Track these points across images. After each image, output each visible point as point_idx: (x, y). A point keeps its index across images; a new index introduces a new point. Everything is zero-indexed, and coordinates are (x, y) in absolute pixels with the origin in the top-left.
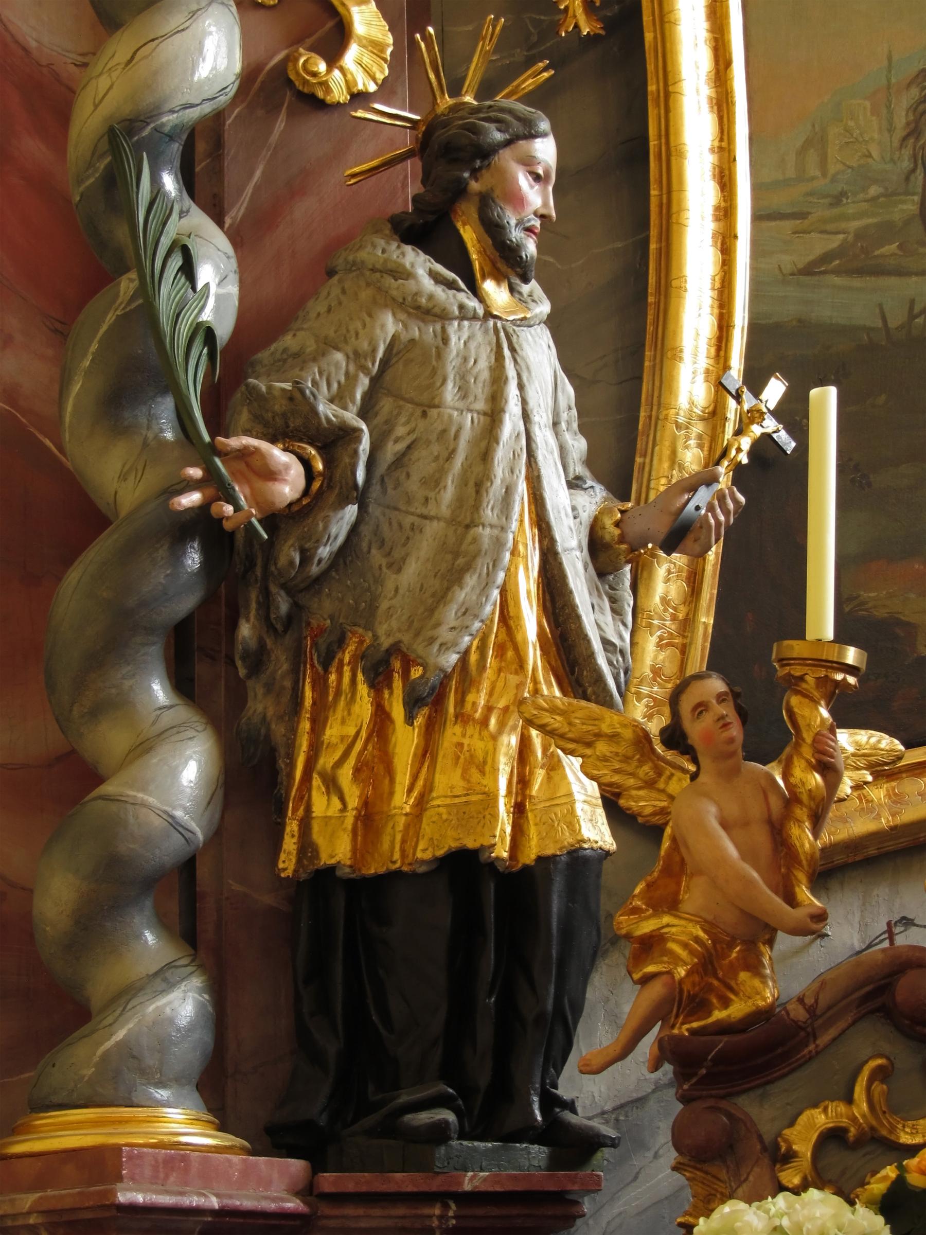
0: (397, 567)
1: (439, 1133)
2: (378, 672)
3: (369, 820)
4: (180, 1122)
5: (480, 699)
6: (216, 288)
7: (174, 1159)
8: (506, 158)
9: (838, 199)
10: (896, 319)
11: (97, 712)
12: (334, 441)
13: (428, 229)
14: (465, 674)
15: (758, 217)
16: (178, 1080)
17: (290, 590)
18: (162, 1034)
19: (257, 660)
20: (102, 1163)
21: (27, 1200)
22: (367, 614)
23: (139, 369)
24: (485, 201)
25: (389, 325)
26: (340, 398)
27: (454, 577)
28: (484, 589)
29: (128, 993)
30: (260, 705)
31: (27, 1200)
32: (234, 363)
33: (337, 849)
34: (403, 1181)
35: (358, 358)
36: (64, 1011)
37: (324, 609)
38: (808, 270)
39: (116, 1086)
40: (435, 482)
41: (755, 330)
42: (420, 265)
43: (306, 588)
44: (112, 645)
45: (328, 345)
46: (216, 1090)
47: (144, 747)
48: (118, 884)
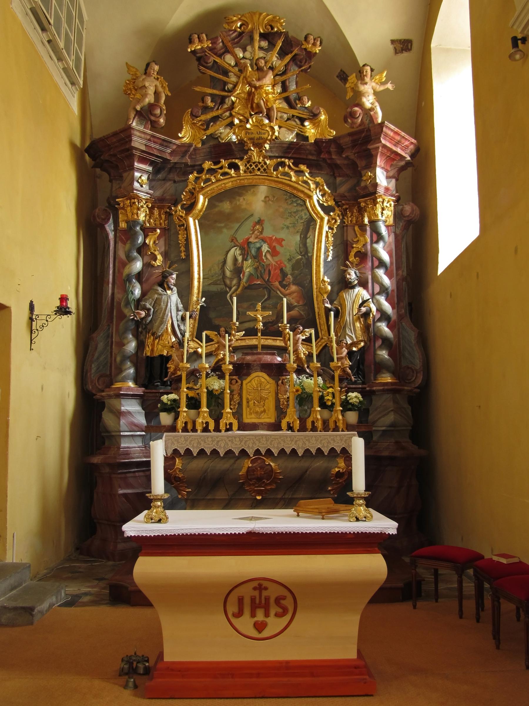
0: (156, 323)
1: (157, 386)
2: (153, 334)
3: (152, 350)
4: (131, 384)
5: (163, 338)
6: (137, 292)
7: (129, 388)
8: (169, 278)
9: (212, 276)
10: (219, 290)
11: (124, 338)
12: (149, 310)
13: (161, 285)
14: (162, 335)
15: (203, 279)
16: (131, 379)
17: (145, 325)
18: (129, 374)
19: (141, 333)
20: (120, 389)
21: (112, 393)
22: (152, 328)
23: (128, 303)
24: (167, 282)
25: (156, 296)
26: (150, 304)
27: (161, 324)
28: (164, 325)
29: (126, 369)
30: (142, 337)
31: (112, 393)
32: (139, 301)
33: (149, 354)
34: (154, 391)
35: (153, 299)
36: (120, 370)
37: (149, 327)
38: (209, 285)
39: (124, 380)
40: (160, 314)
41: (203, 292)
42: (160, 289)
43: (146, 325)
44: (125, 331)
45: (150, 298)
46: (136, 381)
47: (128, 343)
48: (125, 358)
